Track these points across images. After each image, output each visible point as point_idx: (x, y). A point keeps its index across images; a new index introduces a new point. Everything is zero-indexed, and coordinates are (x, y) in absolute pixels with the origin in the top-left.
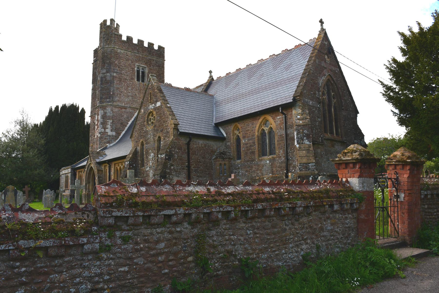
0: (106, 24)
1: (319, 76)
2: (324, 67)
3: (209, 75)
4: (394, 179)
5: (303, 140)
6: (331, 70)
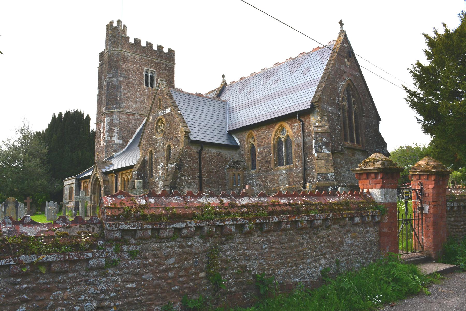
0: (113, 26)
1: (339, 81)
2: (344, 71)
3: (221, 79)
4: (419, 190)
5: (321, 149)
6: (351, 75)
